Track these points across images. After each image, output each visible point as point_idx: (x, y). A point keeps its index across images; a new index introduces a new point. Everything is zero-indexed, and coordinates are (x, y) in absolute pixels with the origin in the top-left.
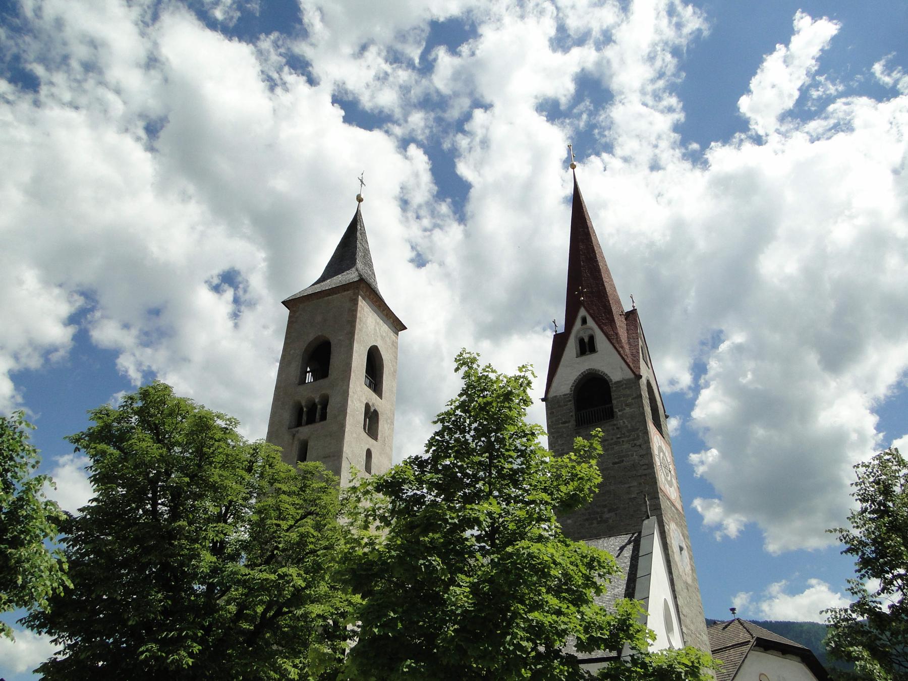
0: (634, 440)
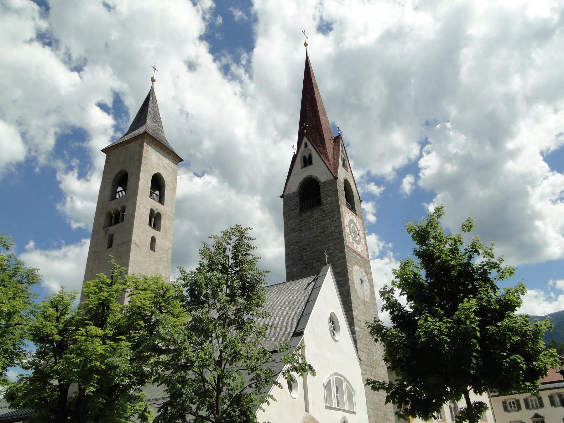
0: (332, 217)
